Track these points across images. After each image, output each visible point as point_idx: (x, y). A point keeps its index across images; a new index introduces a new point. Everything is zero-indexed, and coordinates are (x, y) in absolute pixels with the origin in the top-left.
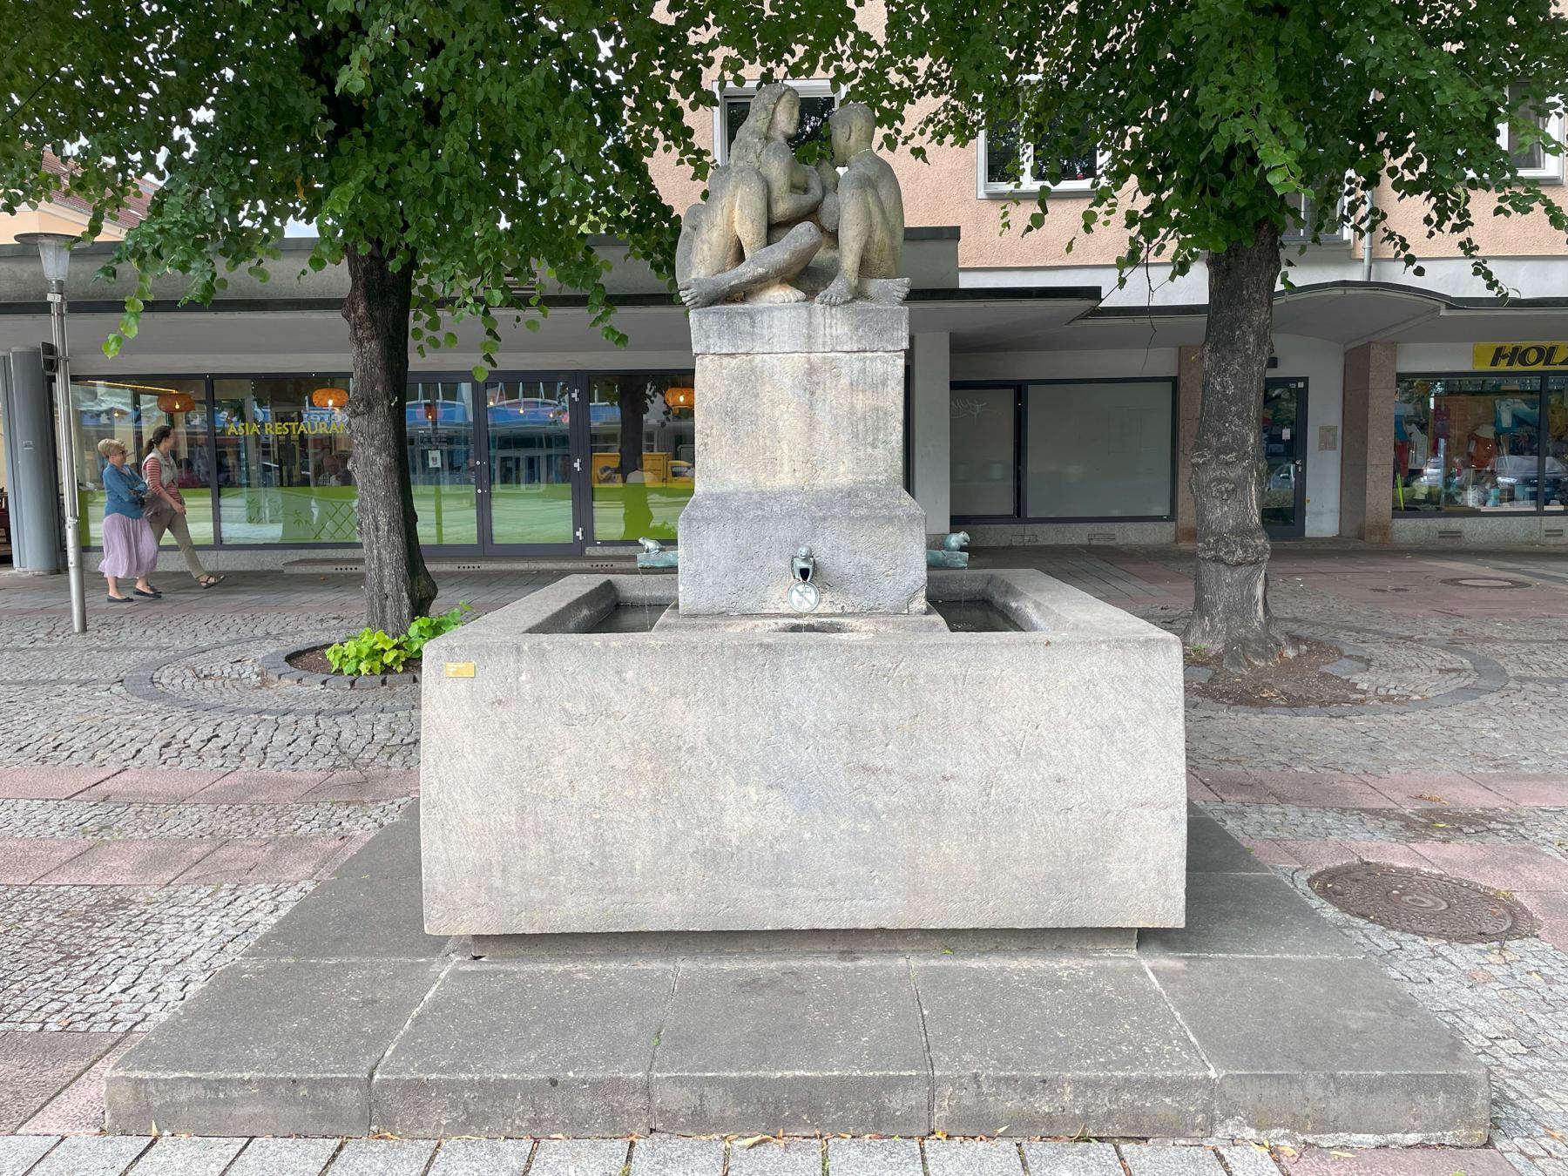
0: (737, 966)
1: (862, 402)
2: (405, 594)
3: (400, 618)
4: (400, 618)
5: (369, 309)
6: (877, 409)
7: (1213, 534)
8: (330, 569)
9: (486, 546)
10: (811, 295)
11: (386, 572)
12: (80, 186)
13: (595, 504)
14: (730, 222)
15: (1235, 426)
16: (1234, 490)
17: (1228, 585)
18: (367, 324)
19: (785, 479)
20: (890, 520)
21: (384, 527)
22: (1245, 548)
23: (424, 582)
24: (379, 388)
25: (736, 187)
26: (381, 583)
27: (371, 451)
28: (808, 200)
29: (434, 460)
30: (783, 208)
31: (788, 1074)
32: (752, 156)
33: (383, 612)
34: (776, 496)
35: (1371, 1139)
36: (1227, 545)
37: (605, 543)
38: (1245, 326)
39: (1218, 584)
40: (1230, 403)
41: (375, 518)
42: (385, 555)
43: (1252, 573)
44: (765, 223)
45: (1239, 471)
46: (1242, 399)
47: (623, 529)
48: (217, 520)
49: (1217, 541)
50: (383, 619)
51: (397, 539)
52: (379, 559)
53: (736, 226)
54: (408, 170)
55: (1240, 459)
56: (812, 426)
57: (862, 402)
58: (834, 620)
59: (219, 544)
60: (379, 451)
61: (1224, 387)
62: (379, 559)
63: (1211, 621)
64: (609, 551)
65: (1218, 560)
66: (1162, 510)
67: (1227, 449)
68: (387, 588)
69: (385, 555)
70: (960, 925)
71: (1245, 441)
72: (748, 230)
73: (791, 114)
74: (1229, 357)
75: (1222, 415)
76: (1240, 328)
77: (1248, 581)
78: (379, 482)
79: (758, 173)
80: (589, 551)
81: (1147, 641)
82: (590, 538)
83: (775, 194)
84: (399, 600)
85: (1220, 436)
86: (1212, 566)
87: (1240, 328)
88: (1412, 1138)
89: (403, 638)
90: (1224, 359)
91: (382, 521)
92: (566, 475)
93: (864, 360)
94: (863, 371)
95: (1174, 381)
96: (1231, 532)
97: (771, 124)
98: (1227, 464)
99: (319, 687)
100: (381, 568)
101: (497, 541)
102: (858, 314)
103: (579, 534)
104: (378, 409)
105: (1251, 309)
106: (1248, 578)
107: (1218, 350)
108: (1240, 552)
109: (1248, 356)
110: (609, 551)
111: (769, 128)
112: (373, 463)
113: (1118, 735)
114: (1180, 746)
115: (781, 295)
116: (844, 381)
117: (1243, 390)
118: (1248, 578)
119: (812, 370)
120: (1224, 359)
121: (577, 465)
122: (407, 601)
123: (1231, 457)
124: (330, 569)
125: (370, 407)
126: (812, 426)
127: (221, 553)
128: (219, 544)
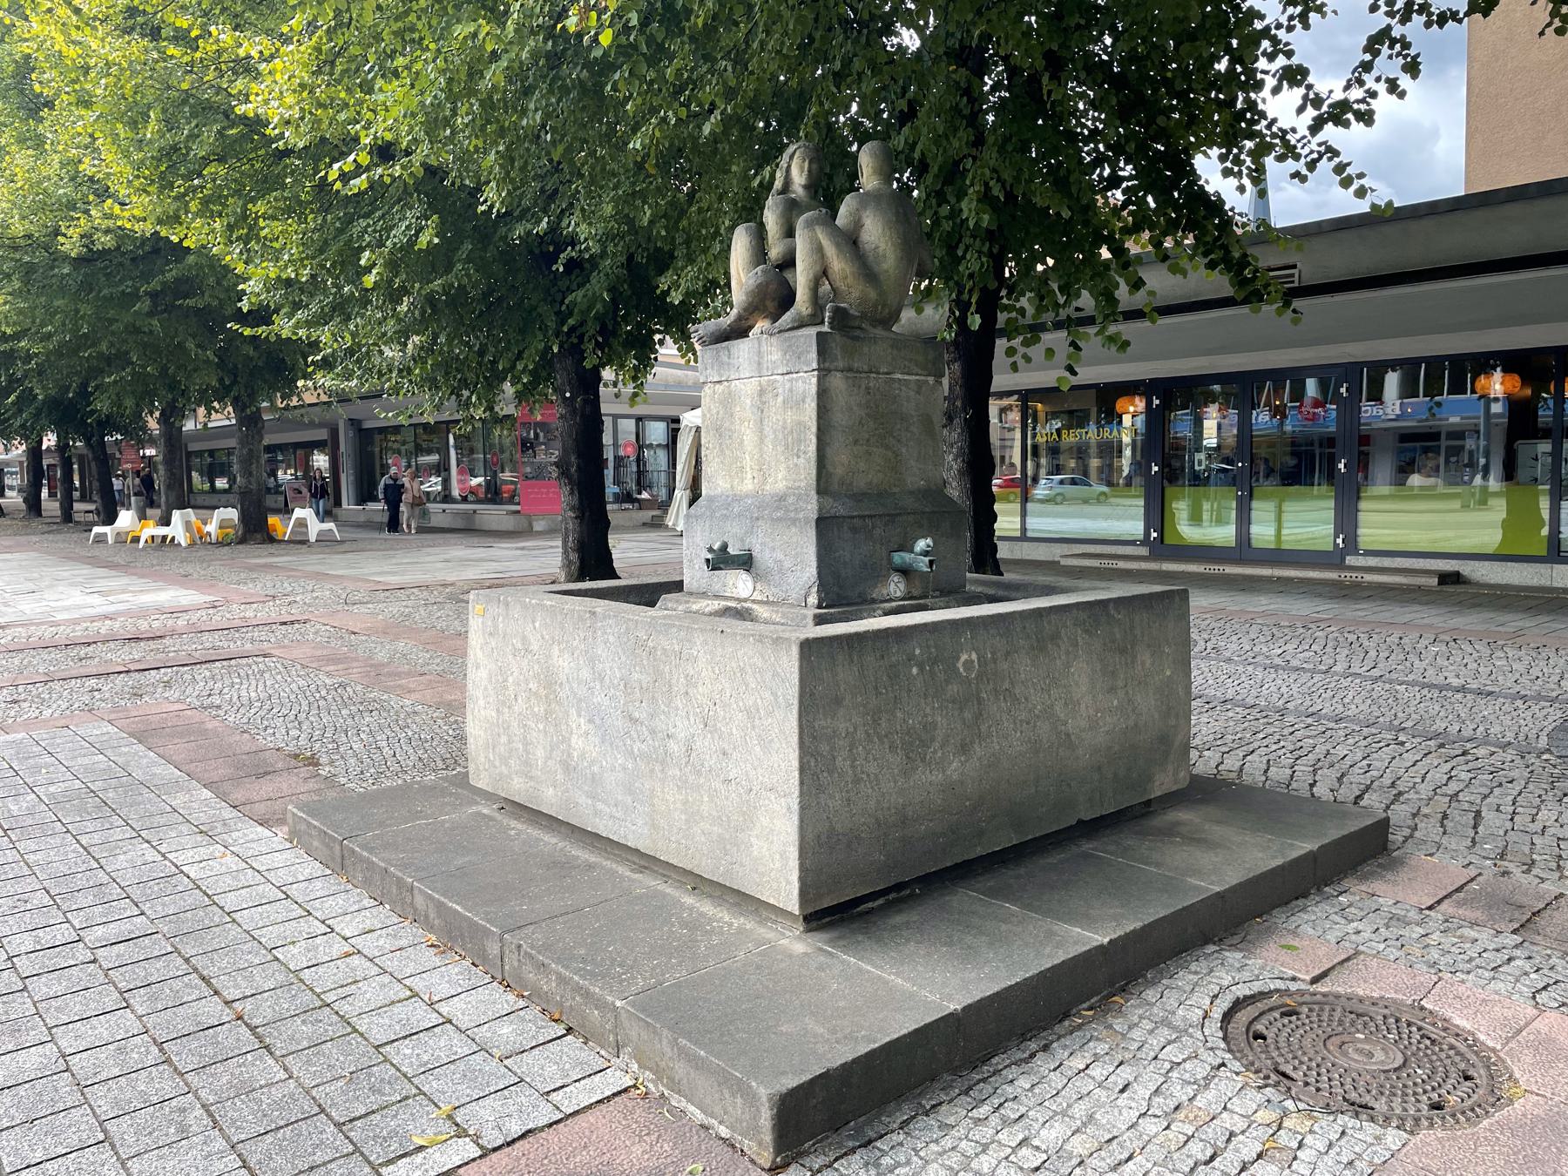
1: (790, 416)
6: (799, 423)
8: (1122, 565)
9: (1243, 550)
13: (1363, 505)
19: (748, 486)
20: (794, 521)
24: (958, 403)
29: (1200, 463)
31: (458, 908)
34: (738, 498)
35: (698, 1116)
37: (1369, 553)
47: (1499, 537)
48: (1024, 514)
56: (762, 440)
57: (790, 416)
58: (746, 605)
59: (1024, 537)
64: (1372, 562)
70: (674, 862)
80: (1350, 560)
81: (778, 638)
82: (1352, 545)
88: (724, 1132)
92: (1331, 475)
93: (791, 381)
94: (791, 390)
101: (1255, 544)
103: (1340, 541)
110: (1372, 562)
113: (757, 722)
114: (795, 739)
116: (780, 399)
119: (762, 392)
121: (1341, 466)
124: (1107, 563)
126: (762, 440)
127: (1025, 544)
128: (1024, 537)
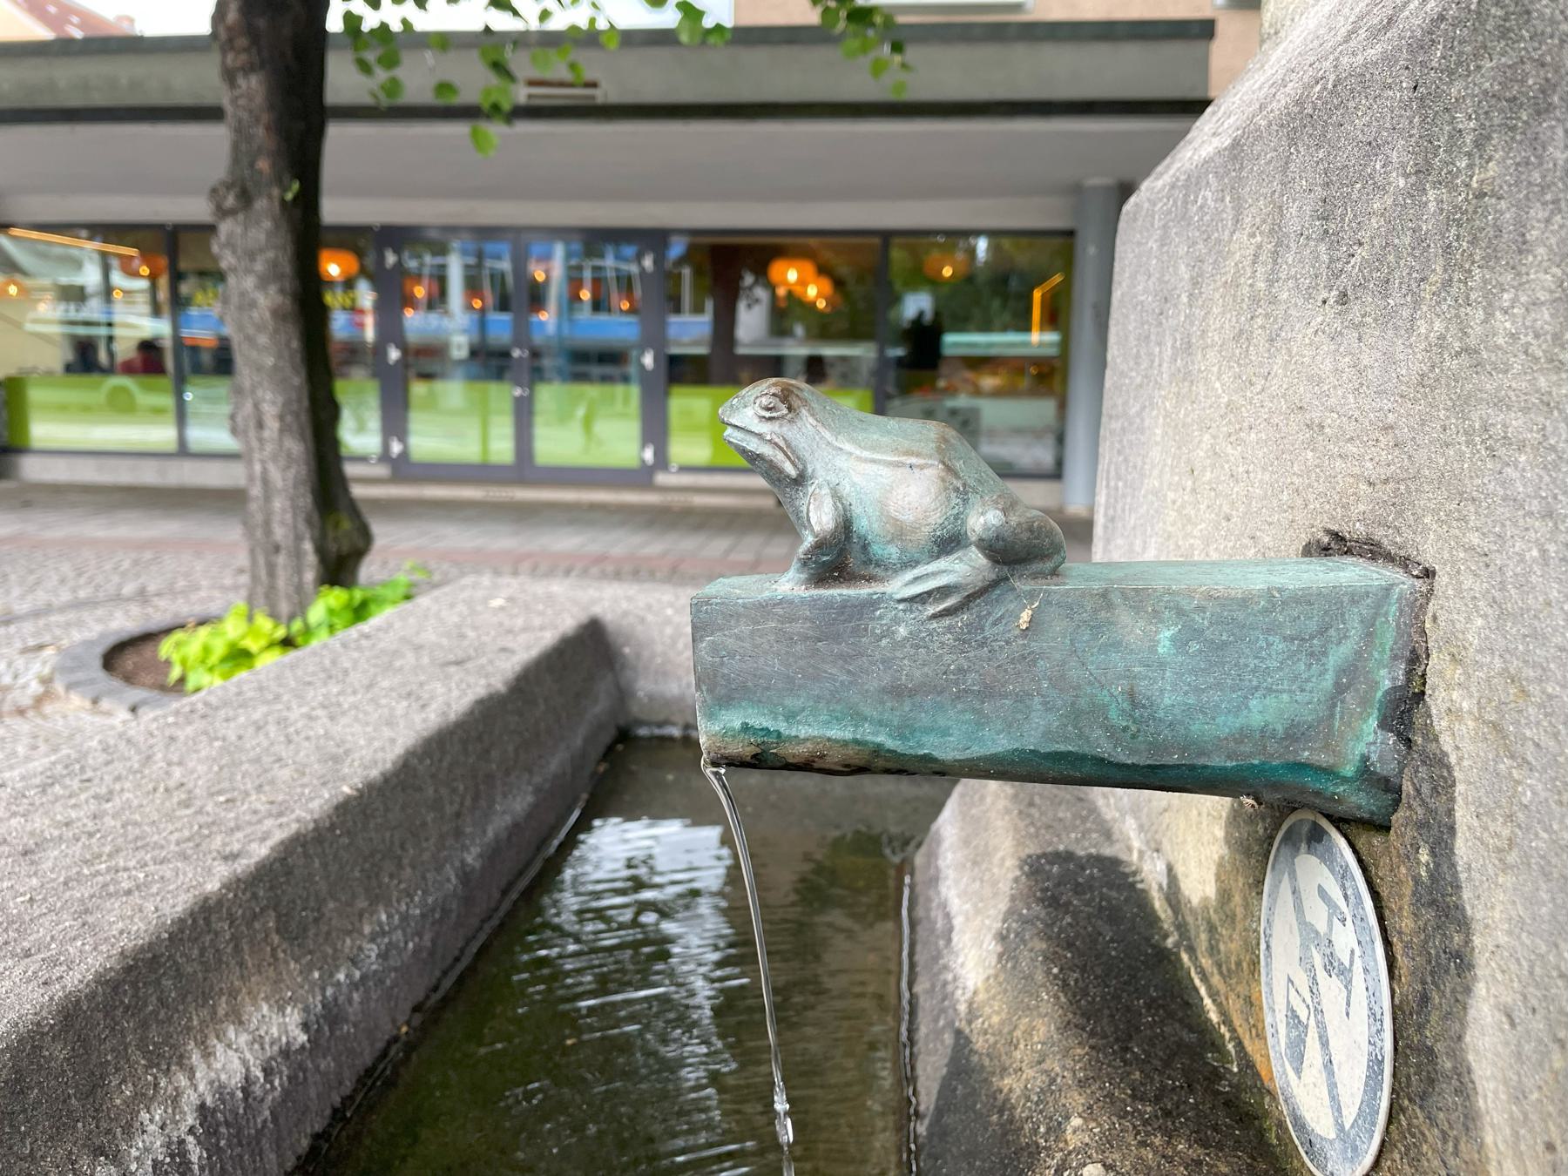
0: (1167, 178)
2: (308, 546)
3: (299, 588)
4: (299, 588)
9: (524, 468)
11: (278, 504)
12: (965, 501)
18: (242, 42)
21: (272, 425)
23: (346, 525)
24: (263, 165)
26: (267, 524)
37: (684, 469)
41: (256, 406)
42: (276, 476)
50: (272, 588)
51: (296, 447)
68: (279, 533)
69: (276, 476)
78: (263, 339)
82: (662, 461)
84: (298, 554)
89: (297, 625)
91: (270, 411)
99: (123, 714)
100: (267, 498)
104: (261, 204)
112: (253, 304)
122: (311, 558)
125: (246, 198)
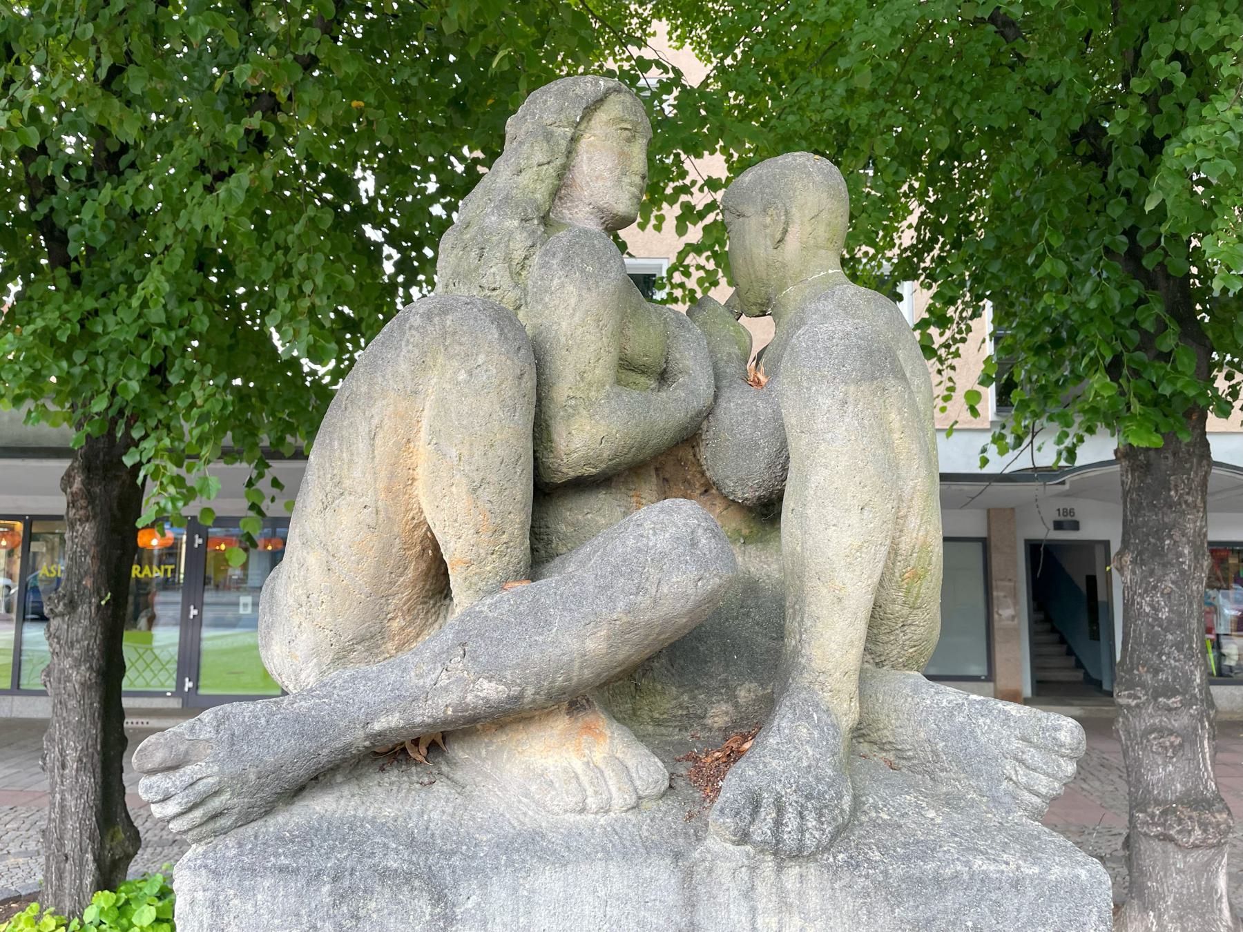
2: (89, 856)
5: (87, 483)
7: (1158, 803)
10: (697, 769)
14: (400, 483)
15: (1173, 660)
16: (1181, 745)
17: (1179, 871)
18: (82, 502)
21: (72, 765)
22: (1204, 826)
24: (88, 582)
25: (422, 365)
26: (61, 839)
27: (67, 663)
28: (667, 410)
30: (582, 439)
32: (496, 273)
33: (60, 878)
36: (1180, 821)
38: (1177, 535)
39: (1165, 868)
40: (1166, 630)
41: (62, 751)
42: (71, 803)
43: (1212, 859)
44: (522, 489)
45: (1186, 720)
46: (1180, 625)
49: (1164, 813)
52: (62, 807)
53: (423, 496)
54: (110, 319)
55: (1187, 704)
60: (77, 664)
61: (1156, 609)
62: (62, 807)
63: (1159, 917)
65: (1167, 838)
66: (979, 669)
67: (1169, 691)
68: (69, 846)
69: (71, 803)
71: (1189, 681)
72: (469, 514)
73: (624, 156)
74: (1158, 572)
75: (1155, 644)
76: (1170, 537)
77: (1207, 869)
78: (72, 703)
79: (505, 319)
83: (563, 390)
84: (82, 864)
85: (1156, 671)
86: (1158, 846)
87: (1170, 537)
90: (1152, 573)
91: (72, 755)
95: (985, 542)
96: (1179, 800)
97: (561, 187)
98: (1170, 709)
102: (895, 897)
104: (82, 609)
105: (1183, 513)
106: (1208, 864)
107: (1143, 563)
108: (1198, 832)
109: (1183, 572)
111: (556, 194)
112: (68, 679)
115: (577, 773)
117: (1181, 614)
118: (1208, 864)
120: (1152, 573)
122: (91, 866)
123: (1174, 701)
